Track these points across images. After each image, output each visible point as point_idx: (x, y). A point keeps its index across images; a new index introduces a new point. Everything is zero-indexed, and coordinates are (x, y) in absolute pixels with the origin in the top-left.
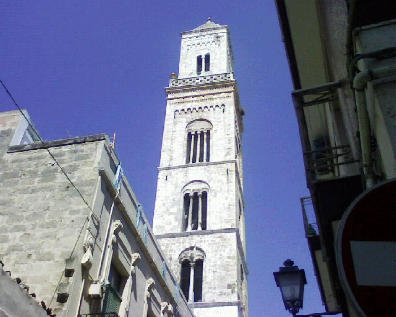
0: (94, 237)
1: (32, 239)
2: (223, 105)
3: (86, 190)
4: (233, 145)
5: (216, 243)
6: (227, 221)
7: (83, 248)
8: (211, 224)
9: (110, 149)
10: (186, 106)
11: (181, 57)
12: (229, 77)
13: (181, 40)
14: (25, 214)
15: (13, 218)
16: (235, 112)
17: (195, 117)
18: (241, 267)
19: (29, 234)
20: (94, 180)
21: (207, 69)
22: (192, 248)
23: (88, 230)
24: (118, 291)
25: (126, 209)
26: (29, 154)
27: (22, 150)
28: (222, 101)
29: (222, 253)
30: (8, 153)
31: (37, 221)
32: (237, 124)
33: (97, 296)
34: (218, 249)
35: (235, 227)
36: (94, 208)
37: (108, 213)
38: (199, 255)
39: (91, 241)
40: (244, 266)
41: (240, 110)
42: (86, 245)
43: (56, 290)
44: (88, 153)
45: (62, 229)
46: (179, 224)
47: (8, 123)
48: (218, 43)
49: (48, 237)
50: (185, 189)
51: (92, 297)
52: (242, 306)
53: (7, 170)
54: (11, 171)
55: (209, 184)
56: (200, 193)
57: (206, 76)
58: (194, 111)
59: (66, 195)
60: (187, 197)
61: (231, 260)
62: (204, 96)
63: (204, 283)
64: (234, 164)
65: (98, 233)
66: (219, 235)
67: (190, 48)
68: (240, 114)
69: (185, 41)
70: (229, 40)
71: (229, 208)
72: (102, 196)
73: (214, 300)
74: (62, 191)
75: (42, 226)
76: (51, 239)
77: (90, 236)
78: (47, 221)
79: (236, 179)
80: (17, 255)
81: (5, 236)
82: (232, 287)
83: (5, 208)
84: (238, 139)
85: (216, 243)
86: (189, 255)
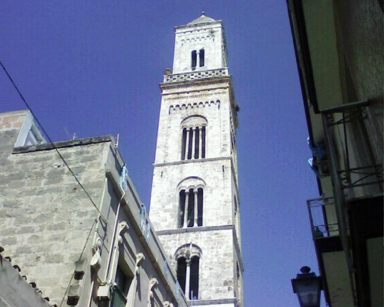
0: (102, 239)
1: (41, 242)
2: (218, 101)
3: (93, 192)
4: (229, 140)
5: (212, 240)
6: (224, 218)
7: (91, 249)
8: (207, 221)
9: (116, 151)
10: (181, 102)
11: (175, 52)
12: (224, 73)
13: (175, 34)
14: (33, 216)
15: (20, 219)
16: (230, 109)
17: (190, 113)
18: (237, 264)
19: (37, 237)
20: (102, 182)
21: (202, 65)
22: (188, 245)
23: (96, 232)
24: (124, 291)
25: (131, 210)
26: (34, 155)
27: (27, 151)
28: (217, 97)
29: (219, 250)
30: (13, 154)
31: (45, 223)
32: (232, 119)
33: (106, 298)
34: (215, 246)
35: (231, 224)
36: (102, 210)
37: (114, 214)
38: (195, 253)
39: (100, 243)
40: (240, 263)
41: (235, 106)
42: (94, 247)
43: (66, 293)
44: (94, 155)
45: (70, 231)
46: (175, 220)
47: (12, 123)
48: (212, 39)
49: (56, 239)
50: (180, 186)
51: (100, 298)
52: (238, 303)
53: (12, 171)
54: (17, 172)
55: (204, 180)
56: (196, 190)
57: (201, 71)
58: (189, 107)
59: (73, 197)
60: (182, 194)
61: (227, 257)
62: (199, 92)
63: (200, 280)
64: (230, 161)
65: (105, 235)
66: (215, 232)
67: (184, 43)
68: (235, 109)
69: (179, 35)
70: (223, 35)
71: (226, 205)
72: (109, 198)
73: (210, 298)
74: (70, 193)
75: (50, 228)
76: (60, 242)
77: (99, 238)
78: (55, 223)
79: (232, 175)
80: (26, 257)
81: (13, 238)
82: (229, 284)
83: (12, 210)
84: (233, 135)
85: (212, 240)
86: (185, 252)
